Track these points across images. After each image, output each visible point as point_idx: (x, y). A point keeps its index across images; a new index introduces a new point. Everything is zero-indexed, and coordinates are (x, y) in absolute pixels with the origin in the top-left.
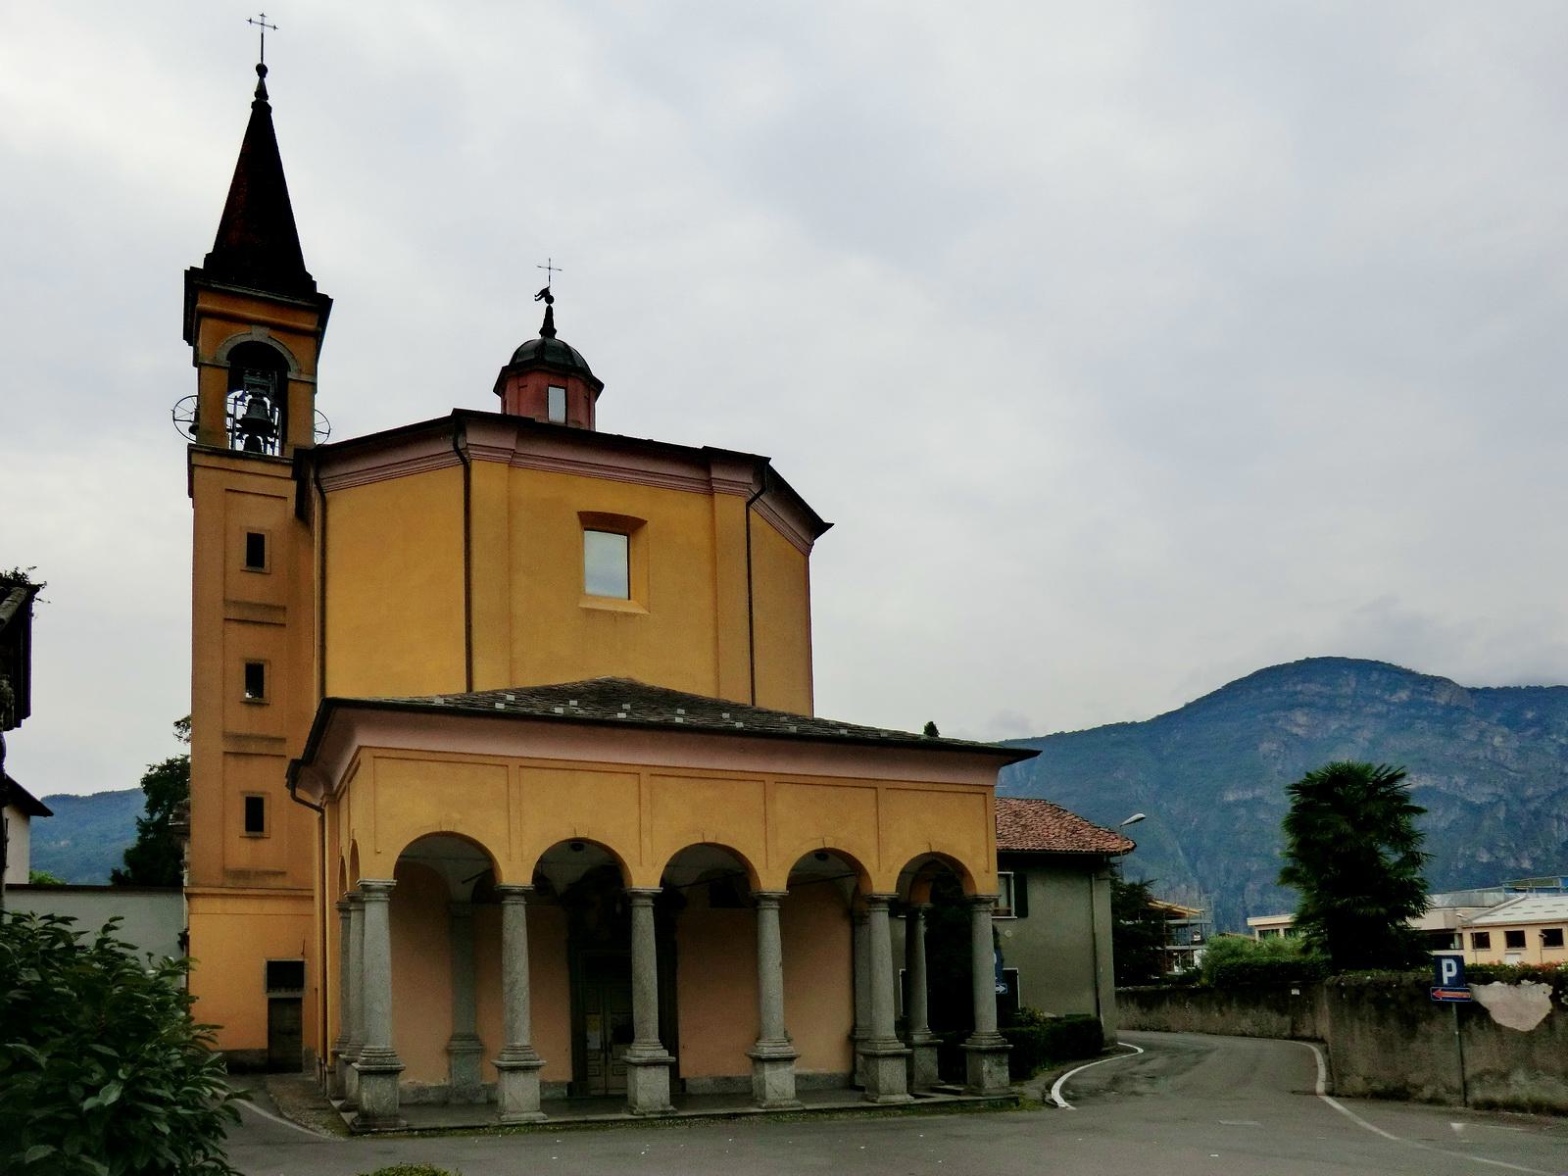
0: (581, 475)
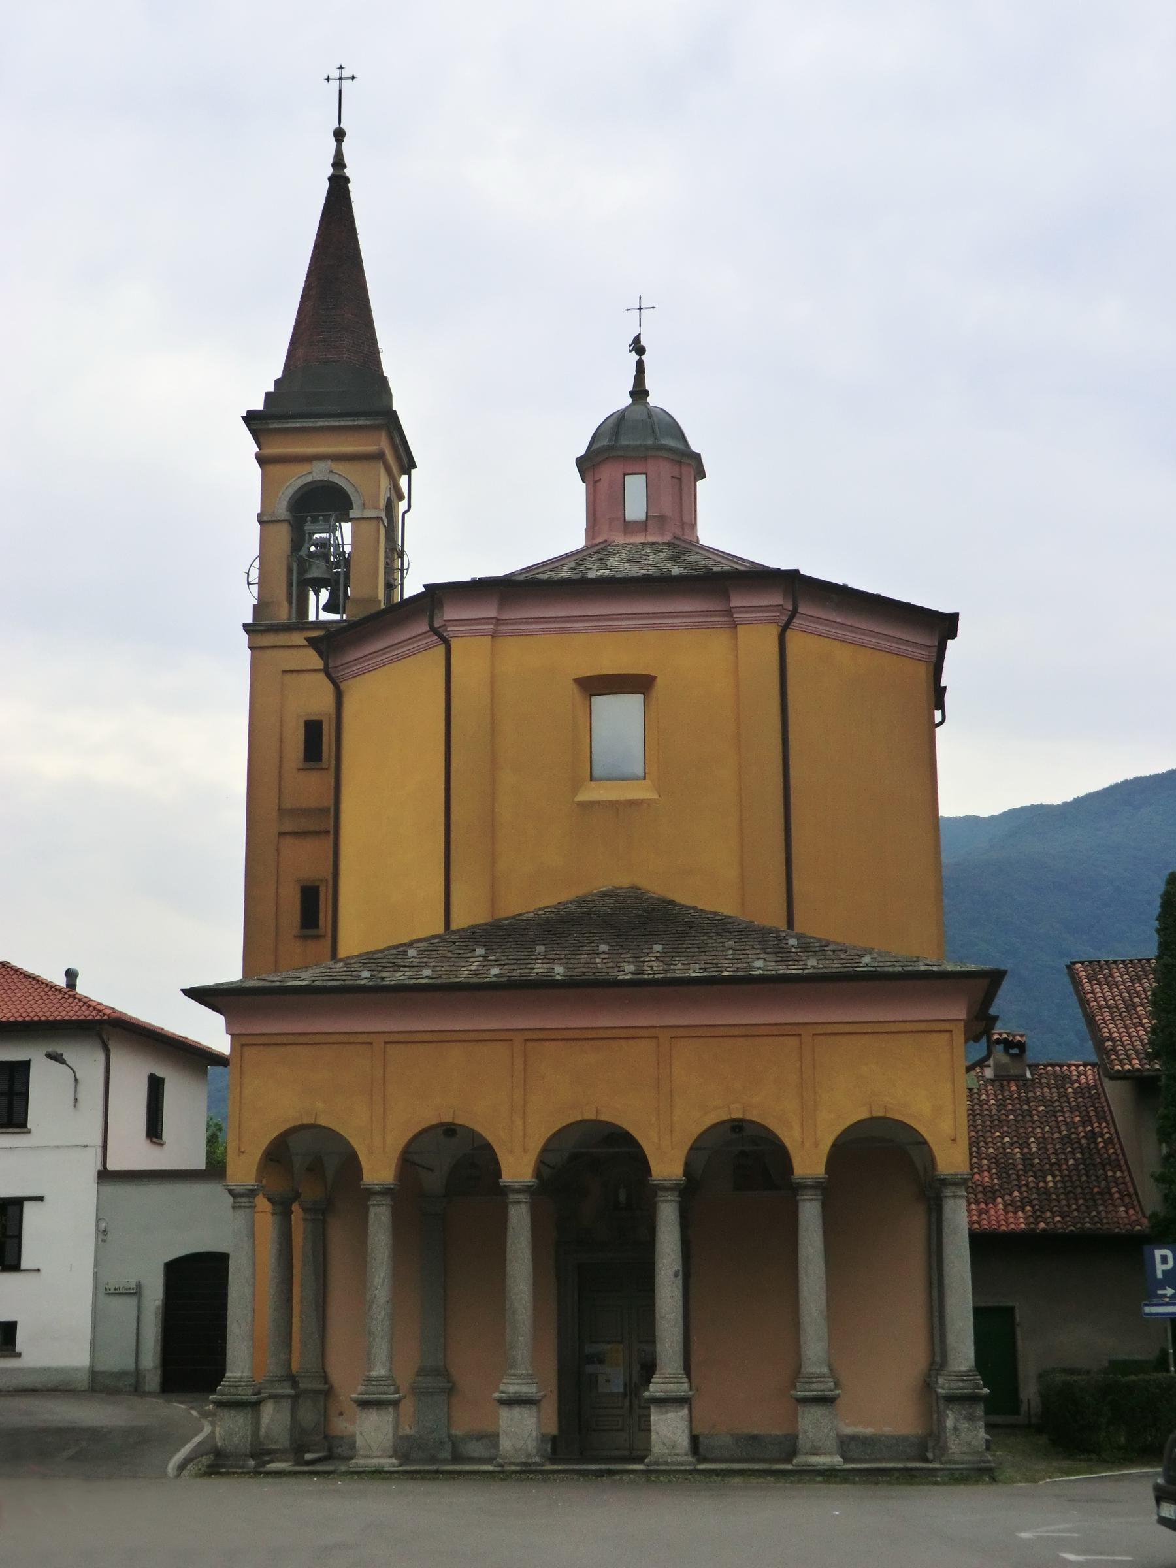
0: (577, 631)
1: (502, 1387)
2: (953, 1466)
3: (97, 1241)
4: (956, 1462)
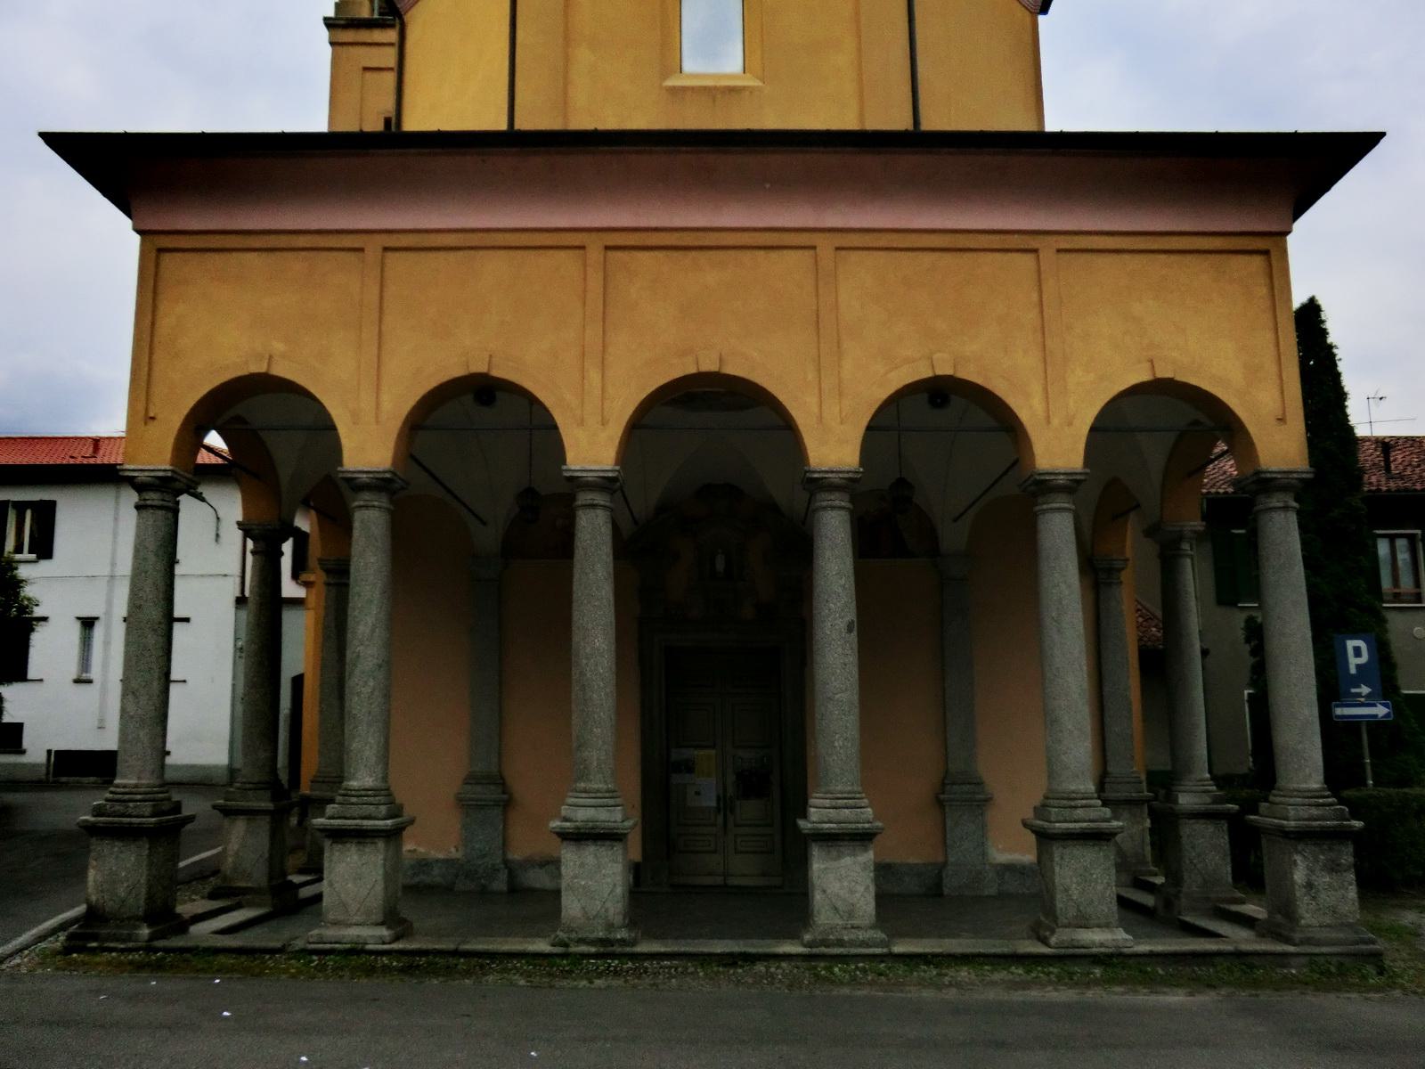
1: (565, 811)
2: (1316, 950)
3: (235, 657)
4: (1318, 943)
